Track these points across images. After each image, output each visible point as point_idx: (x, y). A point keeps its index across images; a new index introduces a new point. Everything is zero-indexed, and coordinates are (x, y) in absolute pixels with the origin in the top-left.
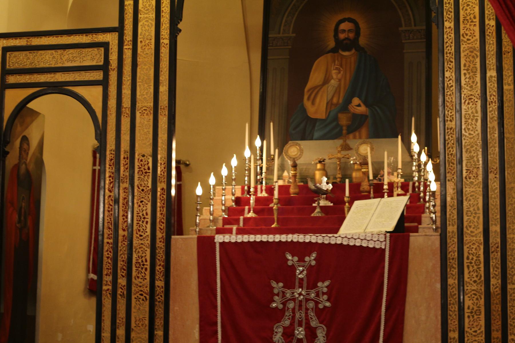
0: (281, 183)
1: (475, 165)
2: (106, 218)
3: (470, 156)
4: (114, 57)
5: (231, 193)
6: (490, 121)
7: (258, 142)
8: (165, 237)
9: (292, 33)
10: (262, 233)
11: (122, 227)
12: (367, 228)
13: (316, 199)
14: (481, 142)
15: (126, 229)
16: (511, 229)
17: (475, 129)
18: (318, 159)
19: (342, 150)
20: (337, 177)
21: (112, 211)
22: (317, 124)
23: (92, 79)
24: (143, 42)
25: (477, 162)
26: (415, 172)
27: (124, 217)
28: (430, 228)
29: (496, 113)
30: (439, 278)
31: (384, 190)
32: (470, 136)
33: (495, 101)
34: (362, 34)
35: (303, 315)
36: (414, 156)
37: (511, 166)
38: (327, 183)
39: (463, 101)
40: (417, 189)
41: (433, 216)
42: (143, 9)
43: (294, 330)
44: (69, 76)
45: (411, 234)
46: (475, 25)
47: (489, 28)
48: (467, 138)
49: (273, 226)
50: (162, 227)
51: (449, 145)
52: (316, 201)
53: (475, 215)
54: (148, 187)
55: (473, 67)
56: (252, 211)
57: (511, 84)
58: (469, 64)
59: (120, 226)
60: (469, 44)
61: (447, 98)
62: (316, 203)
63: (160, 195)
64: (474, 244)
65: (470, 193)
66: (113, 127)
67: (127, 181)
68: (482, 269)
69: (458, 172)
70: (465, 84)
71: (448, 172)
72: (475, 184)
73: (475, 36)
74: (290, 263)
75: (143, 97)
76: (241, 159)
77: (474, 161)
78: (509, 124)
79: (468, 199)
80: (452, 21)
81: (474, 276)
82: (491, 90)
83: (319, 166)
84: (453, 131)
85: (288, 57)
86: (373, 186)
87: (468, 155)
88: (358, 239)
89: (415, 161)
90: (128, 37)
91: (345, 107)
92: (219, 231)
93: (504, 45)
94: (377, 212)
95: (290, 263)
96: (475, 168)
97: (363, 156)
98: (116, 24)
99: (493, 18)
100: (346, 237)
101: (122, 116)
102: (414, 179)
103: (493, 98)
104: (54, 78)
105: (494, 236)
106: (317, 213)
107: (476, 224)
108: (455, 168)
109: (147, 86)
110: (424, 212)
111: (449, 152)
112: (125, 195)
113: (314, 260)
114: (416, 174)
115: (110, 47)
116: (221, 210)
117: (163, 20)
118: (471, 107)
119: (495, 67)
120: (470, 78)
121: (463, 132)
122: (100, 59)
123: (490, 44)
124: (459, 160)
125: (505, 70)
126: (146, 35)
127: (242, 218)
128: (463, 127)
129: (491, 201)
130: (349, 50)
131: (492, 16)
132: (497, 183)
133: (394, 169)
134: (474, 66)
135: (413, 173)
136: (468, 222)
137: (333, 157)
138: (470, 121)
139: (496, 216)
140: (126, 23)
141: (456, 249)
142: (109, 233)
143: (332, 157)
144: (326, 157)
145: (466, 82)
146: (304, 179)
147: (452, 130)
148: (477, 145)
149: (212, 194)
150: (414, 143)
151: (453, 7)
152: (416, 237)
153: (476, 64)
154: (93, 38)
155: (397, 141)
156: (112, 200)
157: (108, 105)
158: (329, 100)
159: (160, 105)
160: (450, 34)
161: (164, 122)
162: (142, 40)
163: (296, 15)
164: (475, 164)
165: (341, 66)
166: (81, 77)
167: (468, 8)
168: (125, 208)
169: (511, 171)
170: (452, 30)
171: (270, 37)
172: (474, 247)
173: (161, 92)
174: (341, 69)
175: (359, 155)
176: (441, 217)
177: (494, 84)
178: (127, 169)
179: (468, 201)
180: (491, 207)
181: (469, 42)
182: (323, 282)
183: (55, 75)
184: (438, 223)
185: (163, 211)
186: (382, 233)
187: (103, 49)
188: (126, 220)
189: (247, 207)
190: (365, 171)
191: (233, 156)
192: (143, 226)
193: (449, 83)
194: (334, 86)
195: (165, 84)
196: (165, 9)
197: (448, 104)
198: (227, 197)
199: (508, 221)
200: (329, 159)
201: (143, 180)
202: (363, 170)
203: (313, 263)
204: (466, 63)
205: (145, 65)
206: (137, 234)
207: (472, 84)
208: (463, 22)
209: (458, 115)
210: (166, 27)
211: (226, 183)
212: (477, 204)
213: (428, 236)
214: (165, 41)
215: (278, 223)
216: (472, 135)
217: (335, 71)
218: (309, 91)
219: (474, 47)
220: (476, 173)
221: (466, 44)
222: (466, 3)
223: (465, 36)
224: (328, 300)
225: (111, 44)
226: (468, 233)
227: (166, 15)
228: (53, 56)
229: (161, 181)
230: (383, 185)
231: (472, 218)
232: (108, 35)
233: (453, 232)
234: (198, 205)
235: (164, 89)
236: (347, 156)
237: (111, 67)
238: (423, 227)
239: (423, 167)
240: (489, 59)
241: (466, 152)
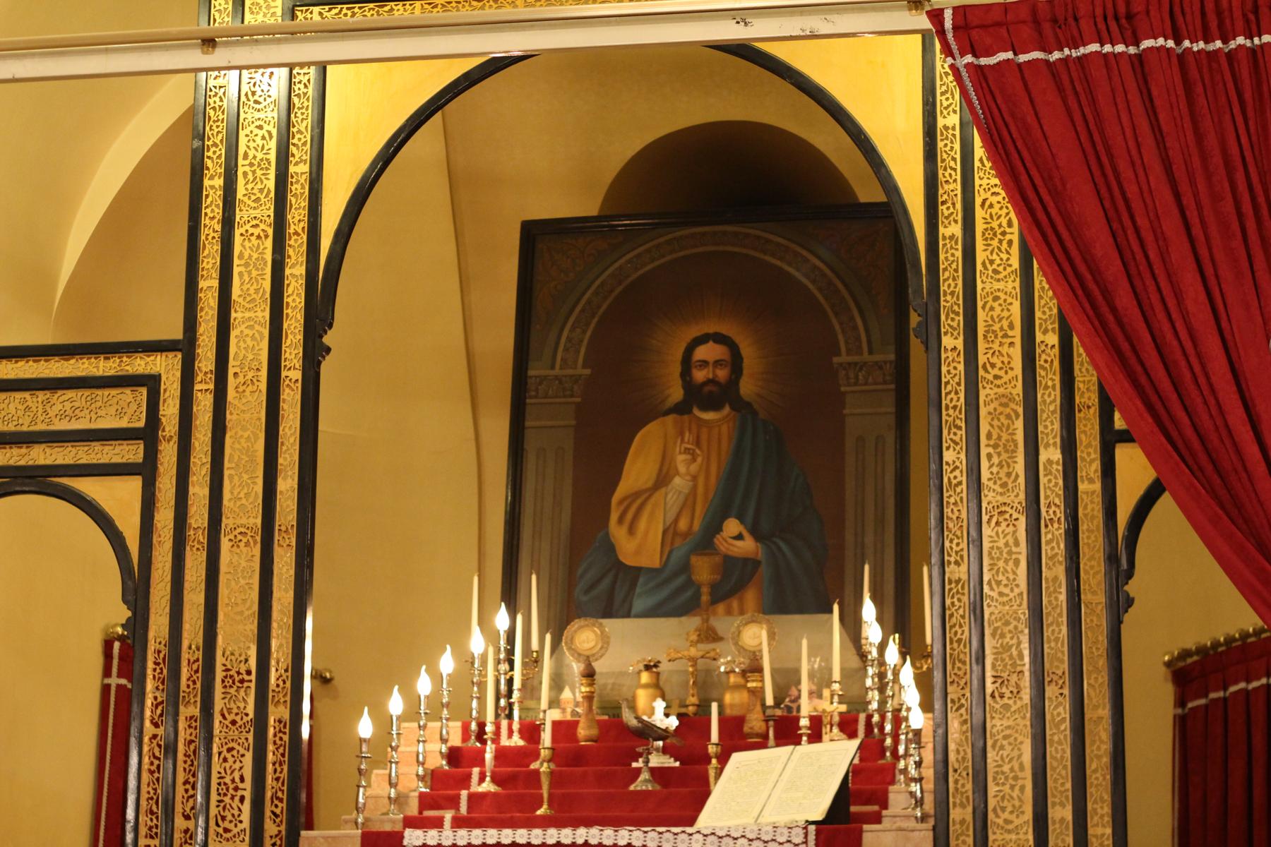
0: (555, 715)
1: (1014, 665)
2: (144, 788)
3: (1002, 644)
4: (170, 410)
5: (438, 736)
6: (1047, 564)
7: (502, 619)
8: (284, 833)
9: (584, 366)
10: (514, 825)
11: (182, 811)
12: (763, 813)
13: (640, 750)
14: (1027, 612)
15: (192, 815)
16: (1097, 814)
17: (1012, 584)
18: (644, 660)
19: (698, 642)
20: (688, 703)
21: (159, 772)
22: (641, 580)
23: (117, 460)
24: (241, 375)
25: (1017, 658)
26: (872, 690)
27: (188, 786)
29: (1062, 546)
31: (800, 728)
32: (1001, 599)
33: (1059, 519)
34: (745, 372)
36: (870, 652)
37: (1098, 668)
38: (667, 715)
39: (985, 518)
40: (876, 730)
41: (915, 788)
42: (240, 300)
44: (62, 454)
45: (866, 827)
46: (1011, 344)
47: (1043, 351)
48: (994, 604)
49: (539, 812)
50: (278, 811)
51: (954, 620)
52: (640, 755)
53: (1014, 783)
54: (247, 715)
55: (1007, 441)
56: (488, 779)
57: (1096, 480)
58: (999, 434)
59: (179, 808)
60: (999, 387)
61: (949, 510)
62: (641, 760)
63: (275, 735)
65: (1002, 731)
66: (165, 574)
67: (196, 702)
69: (975, 682)
70: (989, 479)
71: (952, 682)
72: (1013, 709)
73: (1012, 369)
75: (239, 503)
76: (466, 660)
77: (1011, 657)
78: (1092, 572)
79: (999, 744)
80: (959, 334)
82: (1049, 493)
83: (645, 677)
84: (963, 588)
86: (774, 720)
87: (997, 643)
88: (743, 839)
89: (872, 666)
90: (205, 363)
91: (706, 541)
92: (410, 823)
93: (1079, 389)
96: (1014, 672)
97: (750, 651)
98: (177, 333)
99: (1053, 330)
100: (713, 834)
101: (188, 548)
102: (870, 707)
103: (1054, 512)
104: (26, 458)
105: (1059, 831)
106: (642, 783)
107: (1017, 803)
108: (968, 671)
109: (248, 479)
110: (893, 781)
111: (953, 636)
112: (191, 735)
114: (874, 696)
115: (163, 387)
116: (415, 777)
117: (289, 325)
118: (1003, 532)
119: (1058, 440)
120: (1000, 465)
121: (986, 589)
122: (137, 413)
123: (1046, 387)
124: (977, 653)
125: (1082, 448)
126: (249, 359)
127: (464, 793)
128: (986, 578)
129: (1050, 750)
131: (1051, 324)
132: (1064, 708)
133: (822, 681)
134: (1009, 437)
135: (867, 693)
136: (999, 798)
137: (680, 655)
138: (1001, 564)
139: (1063, 784)
140: (201, 330)
142: (149, 823)
143: (676, 656)
144: (663, 658)
145: (992, 473)
146: (613, 709)
147: (960, 586)
148: (1018, 620)
149: (395, 736)
150: (869, 623)
151: (961, 302)
152: (880, 834)
153: (1014, 434)
154: (123, 365)
155: (831, 619)
156: (160, 746)
157: (155, 521)
158: (668, 524)
159: (277, 524)
160: (955, 364)
161: (286, 562)
162: (237, 370)
163: (592, 326)
164: (1015, 662)
165: (698, 443)
166: (91, 456)
167: (996, 305)
168: (192, 765)
169: (1096, 679)
170: (959, 354)
171: (531, 377)
173: (281, 492)
174: (698, 451)
175: (742, 649)
176: (935, 792)
177: (1056, 478)
178: (197, 671)
179: (997, 748)
180: (1051, 763)
181: (998, 382)
183: (29, 450)
184: (929, 806)
185: (281, 772)
186: (799, 824)
187: (144, 391)
188: (191, 792)
189: (476, 771)
190: (756, 688)
191: (445, 649)
192: (232, 808)
193: (952, 476)
194: (680, 492)
195: (290, 473)
196: (294, 300)
197: (951, 525)
198: (430, 747)
199: (1092, 795)
200: (670, 661)
201: (234, 699)
202: (749, 685)
204: (992, 430)
205: (244, 429)
206: (217, 825)
207: (1005, 479)
208: (985, 337)
209: (973, 553)
210: (294, 341)
211: (428, 711)
212: (1020, 756)
213: (904, 830)
214: (292, 373)
215: (550, 806)
216: (1008, 595)
218: (620, 502)
219: (1010, 393)
220: (1016, 683)
221: (992, 386)
222: (992, 293)
223: (989, 369)
225: (163, 378)
226: (998, 825)
227: (294, 313)
228: (25, 406)
229: (278, 701)
230: (797, 719)
231: (1007, 788)
232: (159, 357)
233: (963, 822)
234: (363, 760)
235: (287, 485)
236: (712, 654)
237: (164, 434)
238: (892, 814)
239: (890, 676)
240: (1045, 421)
241: (993, 635)
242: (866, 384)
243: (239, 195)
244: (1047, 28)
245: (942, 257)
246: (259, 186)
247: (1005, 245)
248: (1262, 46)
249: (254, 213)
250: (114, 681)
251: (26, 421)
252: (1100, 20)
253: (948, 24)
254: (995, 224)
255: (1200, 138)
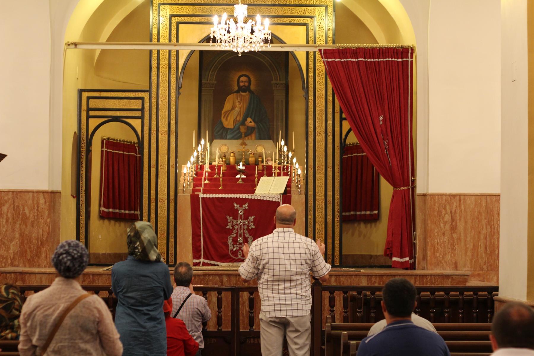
1: (322, 164)
9: (215, 81)
22: (229, 131)
28: (296, 191)
30: (304, 215)
35: (242, 232)
43: (238, 239)
46: (323, 99)
64: (320, 200)
68: (324, 212)
74: (236, 208)
81: (320, 215)
83: (232, 154)
85: (212, 94)
94: (274, 183)
95: (236, 208)
113: (247, 206)
130: (245, 92)
141: (312, 202)
163: (217, 71)
172: (321, 201)
182: (251, 216)
203: (247, 208)
214: (173, 98)
217: (238, 103)
218: (224, 113)
224: (254, 225)
231: (320, 188)
233: (311, 194)
242: (279, 88)
243: (161, 59)
244: (341, 54)
245: (309, 80)
246: (165, 57)
247: (322, 78)
248: (380, 61)
249: (164, 63)
250: (104, 149)
251: (115, 106)
252: (351, 54)
253: (322, 52)
254: (320, 74)
255: (368, 78)
